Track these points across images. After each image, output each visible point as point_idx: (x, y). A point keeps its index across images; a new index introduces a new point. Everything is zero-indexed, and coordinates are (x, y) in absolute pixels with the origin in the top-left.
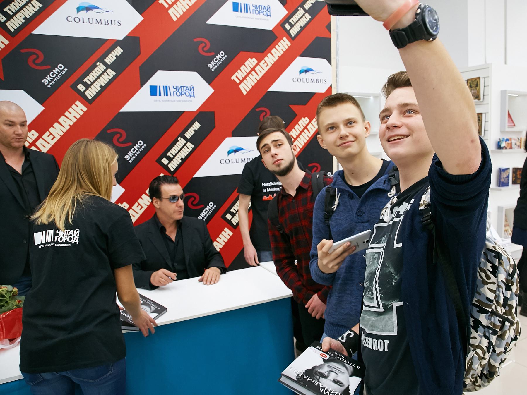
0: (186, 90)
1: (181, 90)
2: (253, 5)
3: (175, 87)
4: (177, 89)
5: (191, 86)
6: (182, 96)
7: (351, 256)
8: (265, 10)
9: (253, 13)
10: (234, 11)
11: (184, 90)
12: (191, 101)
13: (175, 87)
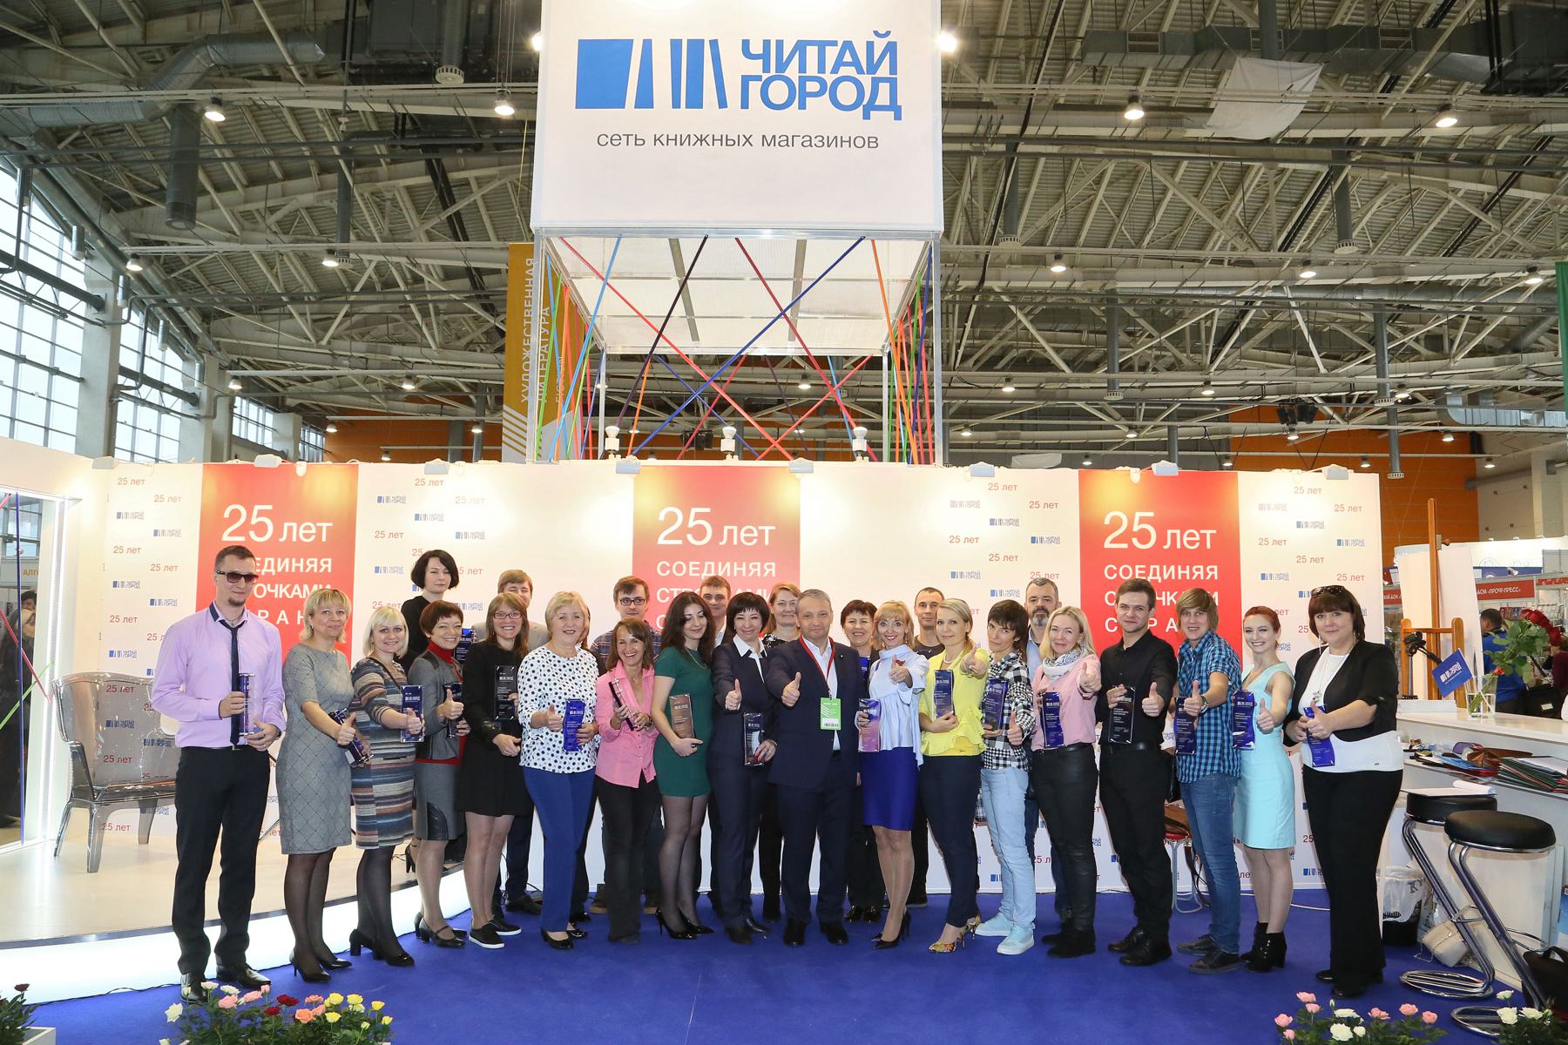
2: (746, 44)
3: (756, 48)
5: (874, 38)
12: (872, 142)
13: (756, 48)
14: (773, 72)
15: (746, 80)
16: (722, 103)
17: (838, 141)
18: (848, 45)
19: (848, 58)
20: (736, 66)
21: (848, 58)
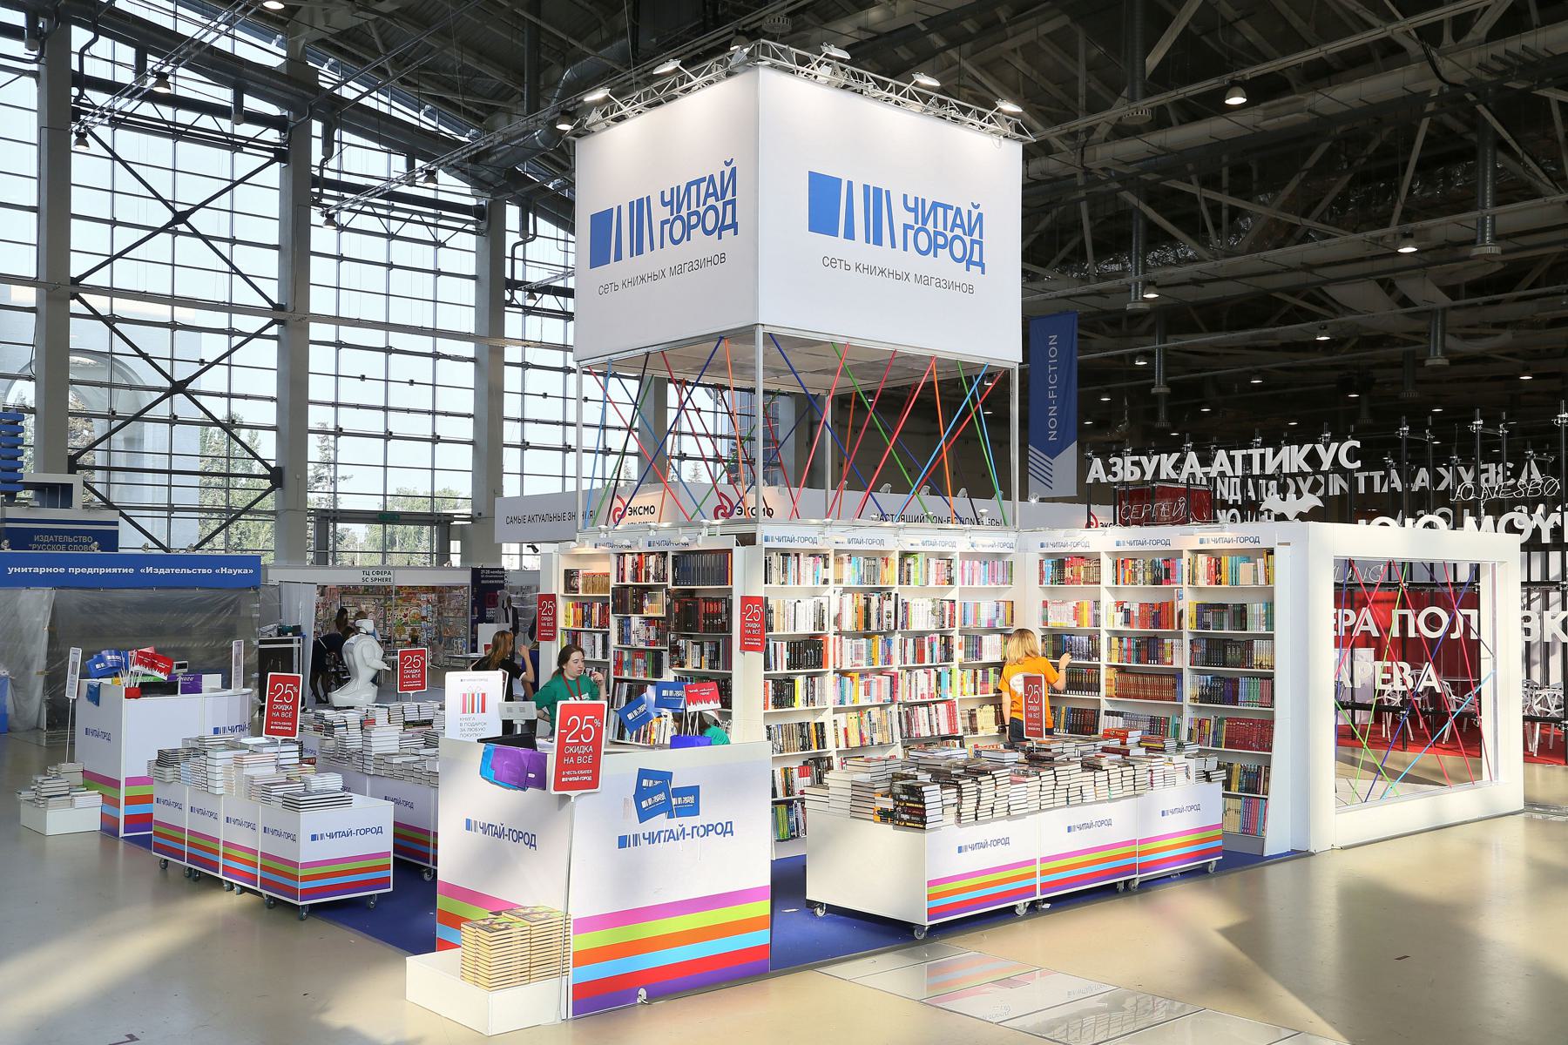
0: (669, 838)
1: (935, 226)
3: (911, 204)
4: (922, 211)
5: (972, 208)
6: (935, 255)
7: (938, 771)
8: (958, 231)
9: (905, 249)
10: (815, 226)
11: (945, 229)
14: (920, 225)
15: (906, 227)
16: (893, 246)
17: (950, 285)
18: (958, 210)
19: (958, 222)
20: (902, 217)
21: (711, 191)
